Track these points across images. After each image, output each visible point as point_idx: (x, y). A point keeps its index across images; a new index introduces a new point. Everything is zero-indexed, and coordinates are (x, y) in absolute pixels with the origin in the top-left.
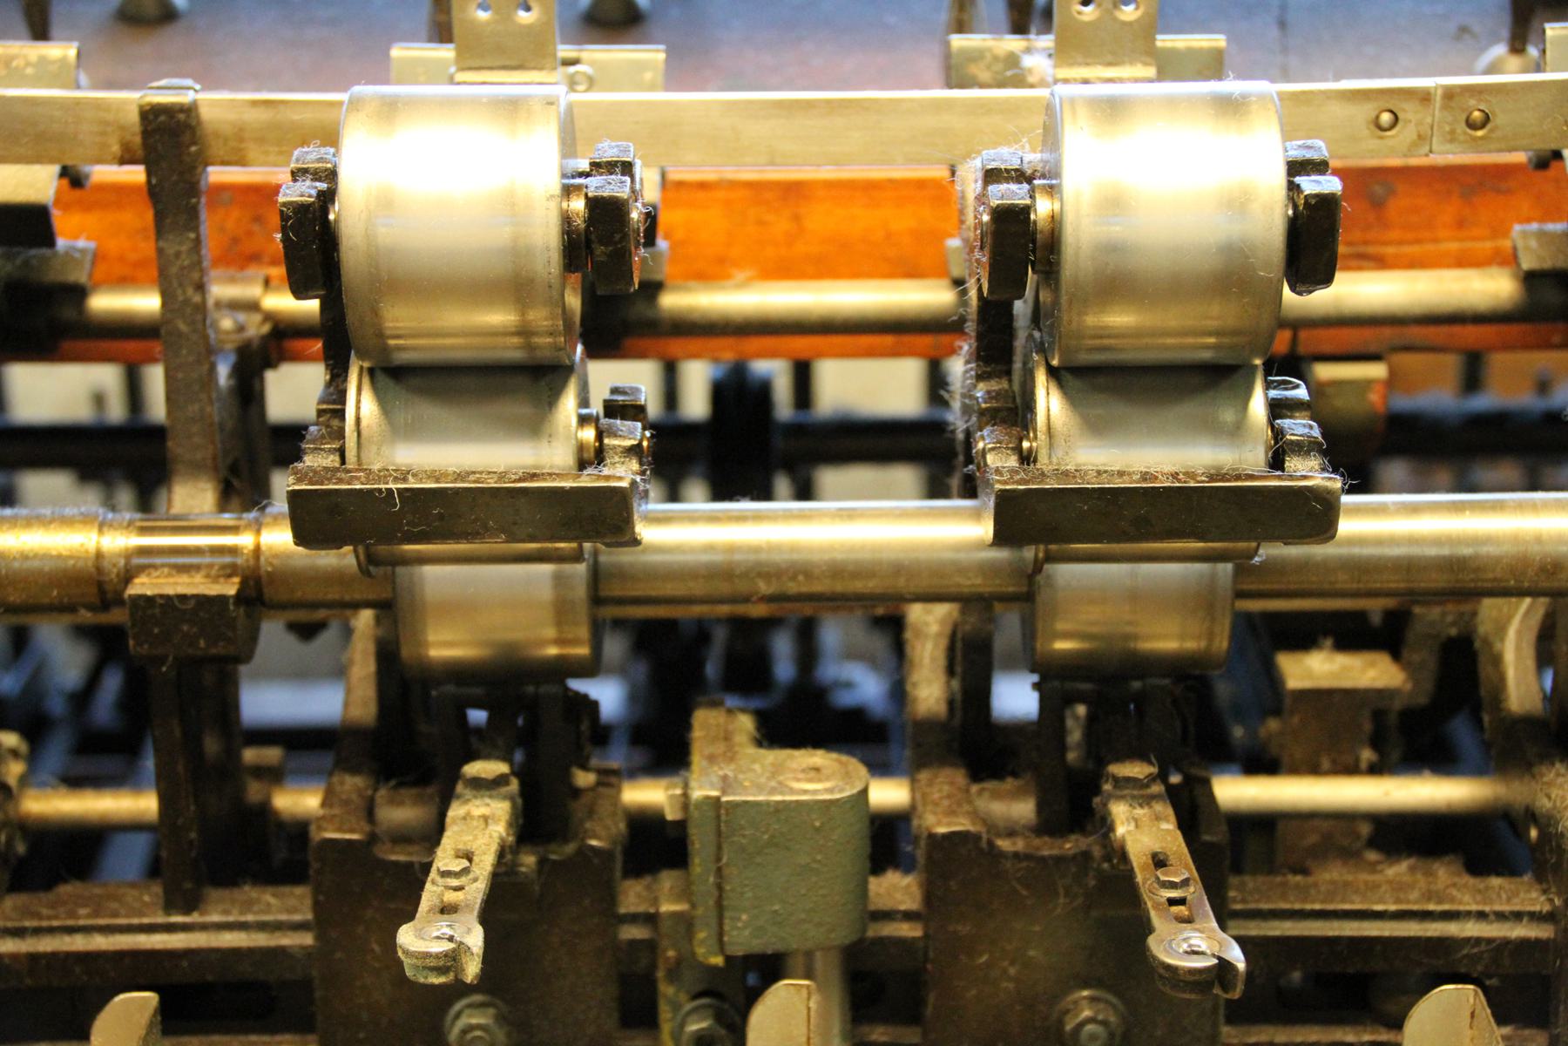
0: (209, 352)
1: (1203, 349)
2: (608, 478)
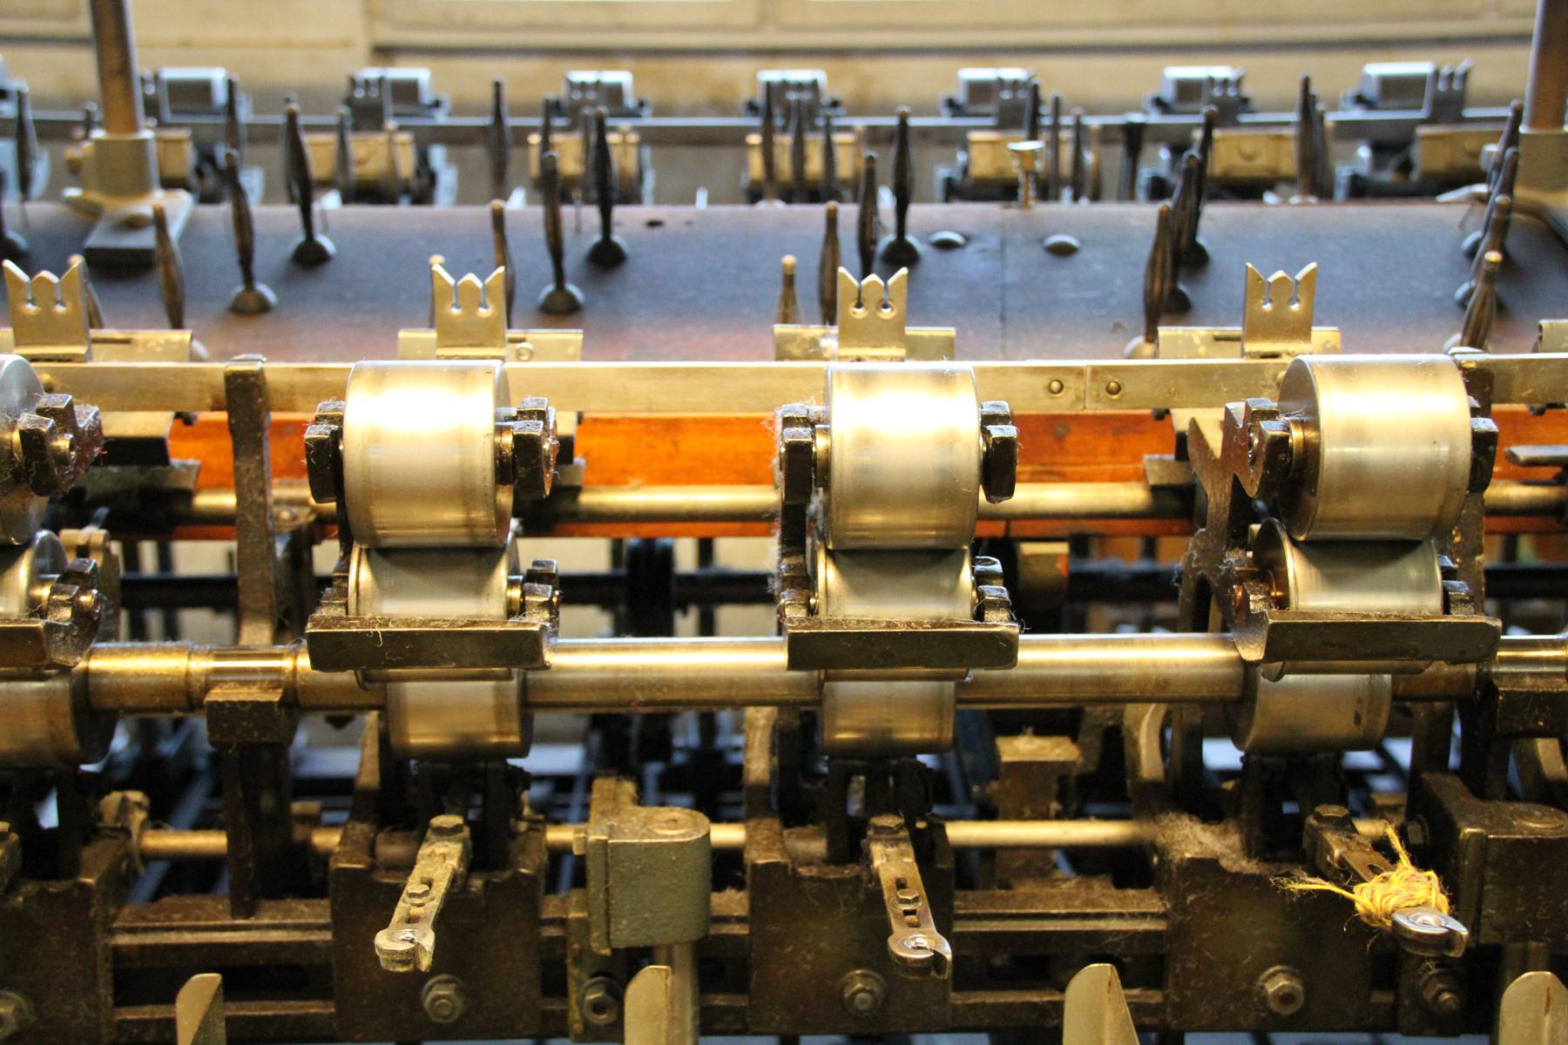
0: (270, 535)
1: (929, 538)
2: (525, 624)
